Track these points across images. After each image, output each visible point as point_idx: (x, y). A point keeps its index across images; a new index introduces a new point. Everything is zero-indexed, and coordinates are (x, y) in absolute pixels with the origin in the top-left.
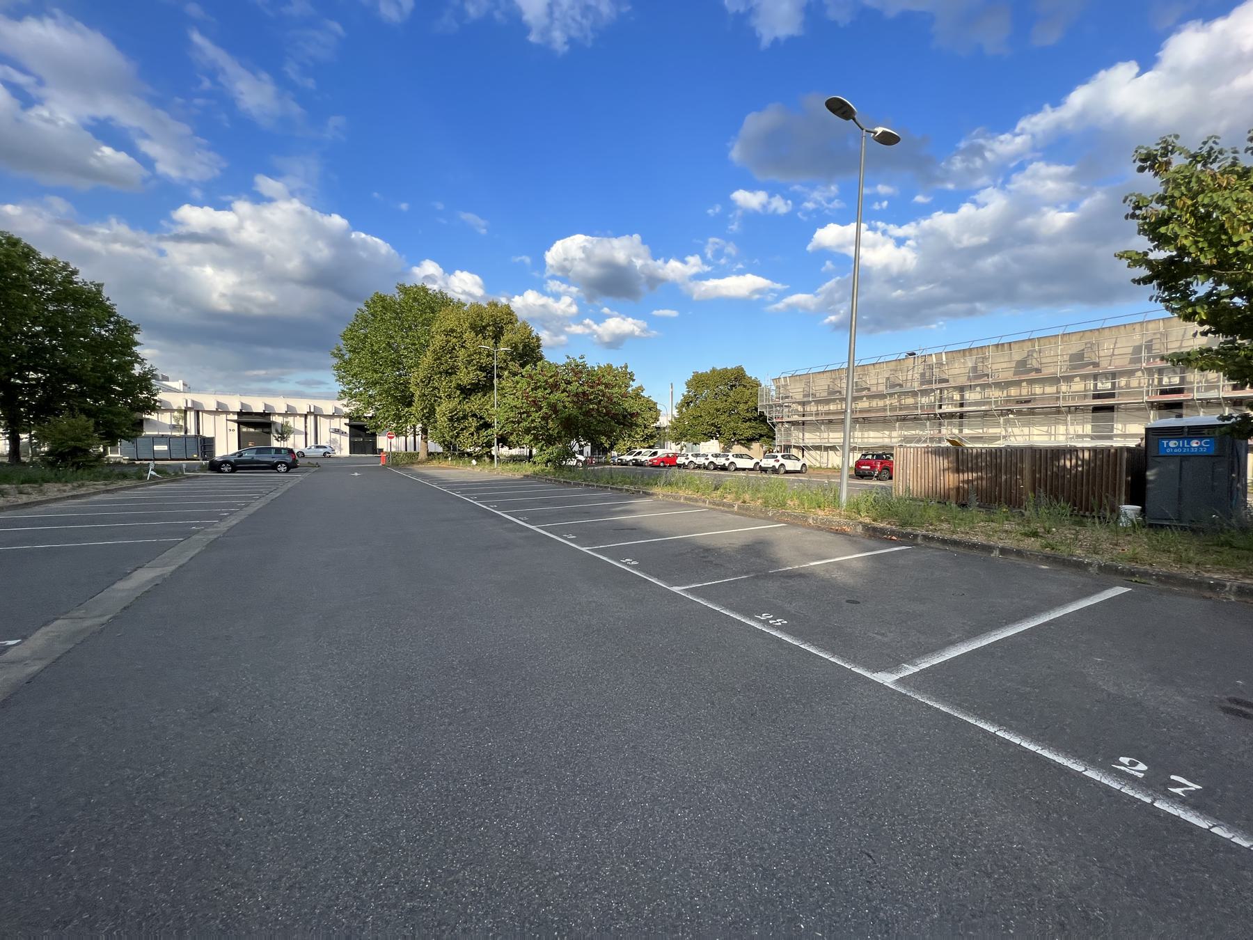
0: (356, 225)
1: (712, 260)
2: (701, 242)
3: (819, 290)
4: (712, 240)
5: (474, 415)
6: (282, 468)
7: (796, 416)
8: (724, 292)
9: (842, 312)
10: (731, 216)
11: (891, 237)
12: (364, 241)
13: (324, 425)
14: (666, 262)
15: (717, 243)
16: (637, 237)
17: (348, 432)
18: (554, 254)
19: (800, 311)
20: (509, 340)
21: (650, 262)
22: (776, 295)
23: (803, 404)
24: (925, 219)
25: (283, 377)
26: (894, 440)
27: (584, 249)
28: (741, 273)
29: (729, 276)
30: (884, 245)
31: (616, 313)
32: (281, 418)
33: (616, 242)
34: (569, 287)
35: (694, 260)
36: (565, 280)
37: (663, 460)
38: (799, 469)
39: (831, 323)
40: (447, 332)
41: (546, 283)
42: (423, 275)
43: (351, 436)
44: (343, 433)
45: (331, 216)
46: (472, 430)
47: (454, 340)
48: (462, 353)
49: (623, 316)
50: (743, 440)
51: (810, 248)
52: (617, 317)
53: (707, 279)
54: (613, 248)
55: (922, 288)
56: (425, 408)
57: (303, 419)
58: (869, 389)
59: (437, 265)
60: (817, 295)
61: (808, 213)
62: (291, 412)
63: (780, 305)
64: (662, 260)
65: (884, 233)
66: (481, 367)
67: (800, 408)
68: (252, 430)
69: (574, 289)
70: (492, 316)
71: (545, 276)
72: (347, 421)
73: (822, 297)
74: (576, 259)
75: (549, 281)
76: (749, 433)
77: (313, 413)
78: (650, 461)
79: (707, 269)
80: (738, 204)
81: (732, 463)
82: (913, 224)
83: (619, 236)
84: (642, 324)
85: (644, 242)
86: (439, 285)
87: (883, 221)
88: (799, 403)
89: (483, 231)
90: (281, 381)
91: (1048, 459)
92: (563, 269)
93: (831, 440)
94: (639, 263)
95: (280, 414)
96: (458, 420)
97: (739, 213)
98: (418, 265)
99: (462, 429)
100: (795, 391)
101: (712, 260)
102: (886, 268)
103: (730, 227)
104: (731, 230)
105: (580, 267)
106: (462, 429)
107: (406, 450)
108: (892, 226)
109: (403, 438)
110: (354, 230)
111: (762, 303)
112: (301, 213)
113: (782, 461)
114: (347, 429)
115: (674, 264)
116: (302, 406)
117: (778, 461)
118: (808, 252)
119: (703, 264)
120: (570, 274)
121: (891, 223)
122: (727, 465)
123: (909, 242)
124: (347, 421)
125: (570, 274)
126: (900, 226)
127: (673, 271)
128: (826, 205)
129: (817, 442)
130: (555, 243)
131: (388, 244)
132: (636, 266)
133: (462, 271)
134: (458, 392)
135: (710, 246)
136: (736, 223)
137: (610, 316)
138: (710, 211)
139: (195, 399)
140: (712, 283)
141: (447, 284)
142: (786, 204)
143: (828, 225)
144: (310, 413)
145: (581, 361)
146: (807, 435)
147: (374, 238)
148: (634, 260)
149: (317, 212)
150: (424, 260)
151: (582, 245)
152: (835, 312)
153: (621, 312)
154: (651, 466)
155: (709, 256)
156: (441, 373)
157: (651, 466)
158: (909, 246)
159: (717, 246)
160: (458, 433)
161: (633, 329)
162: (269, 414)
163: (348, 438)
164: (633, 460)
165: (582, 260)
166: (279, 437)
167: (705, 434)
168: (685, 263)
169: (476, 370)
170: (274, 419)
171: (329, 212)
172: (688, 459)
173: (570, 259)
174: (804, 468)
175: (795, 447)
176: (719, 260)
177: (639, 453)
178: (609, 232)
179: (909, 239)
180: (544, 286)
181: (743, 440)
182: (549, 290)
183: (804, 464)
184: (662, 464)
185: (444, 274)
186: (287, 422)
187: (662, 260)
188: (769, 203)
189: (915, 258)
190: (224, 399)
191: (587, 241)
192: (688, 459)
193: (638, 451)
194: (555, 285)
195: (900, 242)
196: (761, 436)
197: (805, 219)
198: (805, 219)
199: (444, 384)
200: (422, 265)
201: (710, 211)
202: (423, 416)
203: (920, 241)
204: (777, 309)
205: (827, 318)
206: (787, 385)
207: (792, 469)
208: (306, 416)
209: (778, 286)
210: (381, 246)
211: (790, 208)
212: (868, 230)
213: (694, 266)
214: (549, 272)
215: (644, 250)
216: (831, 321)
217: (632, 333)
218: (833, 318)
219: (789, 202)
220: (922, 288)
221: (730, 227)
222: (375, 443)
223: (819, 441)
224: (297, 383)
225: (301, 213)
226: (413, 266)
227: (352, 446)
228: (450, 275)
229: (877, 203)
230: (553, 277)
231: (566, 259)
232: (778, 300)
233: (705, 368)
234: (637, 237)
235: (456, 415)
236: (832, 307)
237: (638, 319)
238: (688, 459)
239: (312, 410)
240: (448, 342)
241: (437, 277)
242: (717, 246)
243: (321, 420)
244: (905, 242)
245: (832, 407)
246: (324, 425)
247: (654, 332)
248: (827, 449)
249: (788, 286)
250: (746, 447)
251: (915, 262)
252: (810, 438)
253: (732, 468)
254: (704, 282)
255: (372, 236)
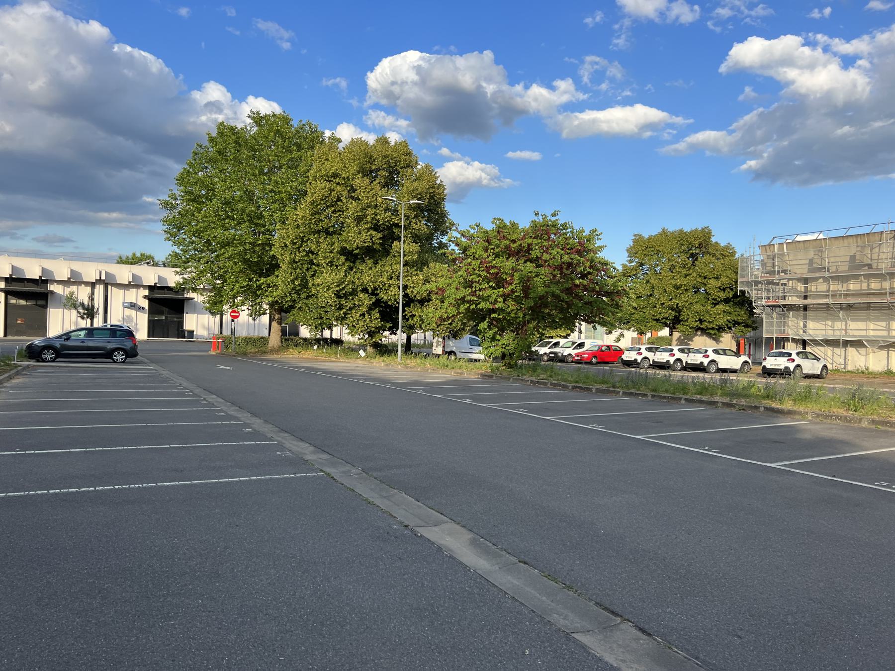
0: (120, 34)
1: (589, 85)
2: (577, 62)
3: (734, 125)
4: (589, 58)
5: (365, 290)
6: (119, 357)
7: (795, 298)
8: (604, 127)
9: (765, 155)
10: (616, 27)
11: (835, 54)
12: (130, 55)
13: (117, 297)
14: (527, 87)
15: (596, 63)
16: (488, 55)
17: (147, 307)
18: (378, 75)
19: (708, 153)
20: (413, 191)
21: (505, 87)
22: (675, 132)
23: (806, 281)
24: (883, 32)
25: (16, 231)
26: (838, 333)
27: (418, 69)
28: (628, 102)
29: (612, 107)
30: (825, 65)
31: (458, 155)
32: (61, 287)
33: (461, 62)
34: (397, 120)
35: (564, 85)
36: (390, 110)
37: (594, 354)
38: (819, 372)
39: (749, 170)
40: (328, 177)
41: (366, 113)
42: (205, 102)
43: (151, 312)
44: (141, 309)
45: (88, 22)
46: (364, 309)
47: (339, 188)
48: (352, 207)
49: (467, 159)
50: (713, 329)
51: (723, 69)
52: (459, 160)
53: (582, 111)
54: (457, 69)
55: (878, 124)
56: (296, 278)
57: (89, 289)
58: (870, 266)
59: (223, 89)
60: (731, 132)
61: (721, 22)
62: (75, 280)
63: (681, 146)
64: (522, 84)
65: (826, 49)
66: (376, 225)
67: (801, 287)
68: (22, 302)
69: (403, 123)
70: (386, 157)
71: (366, 104)
72: (146, 292)
73: (738, 135)
74: (407, 82)
75: (370, 111)
76: (722, 320)
77: (104, 280)
78: (577, 355)
79: (582, 97)
80: (627, 10)
81: (713, 361)
82: (866, 38)
83: (466, 53)
84: (494, 170)
85: (497, 62)
86: (226, 115)
87: (825, 34)
88: (799, 280)
89: (286, 46)
90: (13, 236)
91: (101, 311)
92: (389, 95)
93: (851, 333)
94: (490, 89)
95: (60, 282)
96: (346, 296)
97: (627, 22)
98: (199, 88)
99: (351, 309)
100: (794, 262)
101: (589, 85)
102: (828, 96)
103: (616, 41)
104: (616, 45)
105: (413, 93)
106: (351, 309)
107: (221, 333)
108: (837, 40)
109: (218, 317)
110: (117, 42)
111: (655, 142)
112: (51, 19)
113: (798, 360)
114: (145, 304)
115: (537, 91)
116: (90, 272)
117: (674, 355)
118: (721, 74)
119: (577, 90)
120: (399, 102)
121: (836, 37)
122: (706, 364)
123: (860, 62)
124: (146, 292)
125: (399, 102)
126: (848, 40)
127: (536, 100)
128: (746, 12)
129: (831, 335)
130: (380, 61)
131: (160, 60)
132: (487, 93)
133: (256, 97)
134: (343, 258)
135: (586, 66)
136: (623, 36)
137: (450, 160)
138: (588, 20)
139: (73, 268)
140: (589, 115)
141: (235, 113)
142: (692, 10)
143: (749, 38)
144: (99, 281)
145: (553, 219)
146: (811, 325)
147: (143, 53)
148: (484, 85)
149: (71, 18)
150: (208, 81)
151: (416, 64)
152: (755, 156)
153: (464, 154)
154: (578, 362)
155: (585, 79)
156: (319, 232)
157: (578, 362)
158: (859, 67)
159: (596, 67)
160: (345, 314)
161: (481, 177)
162: (46, 282)
163: (146, 316)
164: (551, 353)
165: (415, 83)
166: (84, 314)
167: (657, 320)
168: (552, 88)
169: (368, 229)
170: (51, 287)
171: (86, 18)
172: (674, 355)
173: (399, 82)
174: (824, 371)
175: (794, 340)
176: (599, 84)
177: (556, 344)
178: (452, 48)
179: (861, 58)
180: (364, 117)
181: (713, 329)
182: (370, 123)
183: (825, 367)
184: (594, 360)
185: (232, 101)
186: (72, 293)
187: (522, 84)
188: (668, 9)
189: (869, 83)
190: (78, 266)
191: (422, 59)
192: (641, 354)
193: (554, 341)
194: (378, 117)
195: (848, 62)
196: (736, 323)
197: (718, 29)
198: (718, 29)
199: (324, 247)
200: (204, 87)
201: (588, 20)
202: (293, 289)
203: (876, 61)
204: (676, 150)
205: (744, 162)
206: (783, 255)
207: (810, 372)
208: (93, 285)
209: (679, 120)
210: (153, 63)
211: (697, 15)
212: (803, 45)
213: (565, 92)
214: (370, 100)
215: (498, 71)
216: (750, 167)
217: (479, 180)
218: (752, 163)
219: (696, 7)
220: (878, 124)
221: (616, 41)
222: (181, 323)
223: (831, 333)
224: (33, 239)
225: (51, 19)
226: (194, 90)
227: (151, 326)
228: (240, 103)
229: (816, 10)
230: (376, 107)
231: (393, 83)
232: (678, 138)
233: (649, 231)
234: (488, 55)
235: (343, 289)
236: (752, 149)
237: (487, 164)
238: (708, 356)
239: (103, 278)
240: (331, 190)
241: (223, 104)
242: (596, 67)
243: (114, 292)
244: (855, 62)
245: (853, 286)
246: (117, 297)
247: (508, 180)
248: (846, 343)
249: (691, 121)
250: (714, 339)
251: (868, 89)
252: (816, 328)
253: (713, 368)
254: (577, 114)
255: (140, 49)
